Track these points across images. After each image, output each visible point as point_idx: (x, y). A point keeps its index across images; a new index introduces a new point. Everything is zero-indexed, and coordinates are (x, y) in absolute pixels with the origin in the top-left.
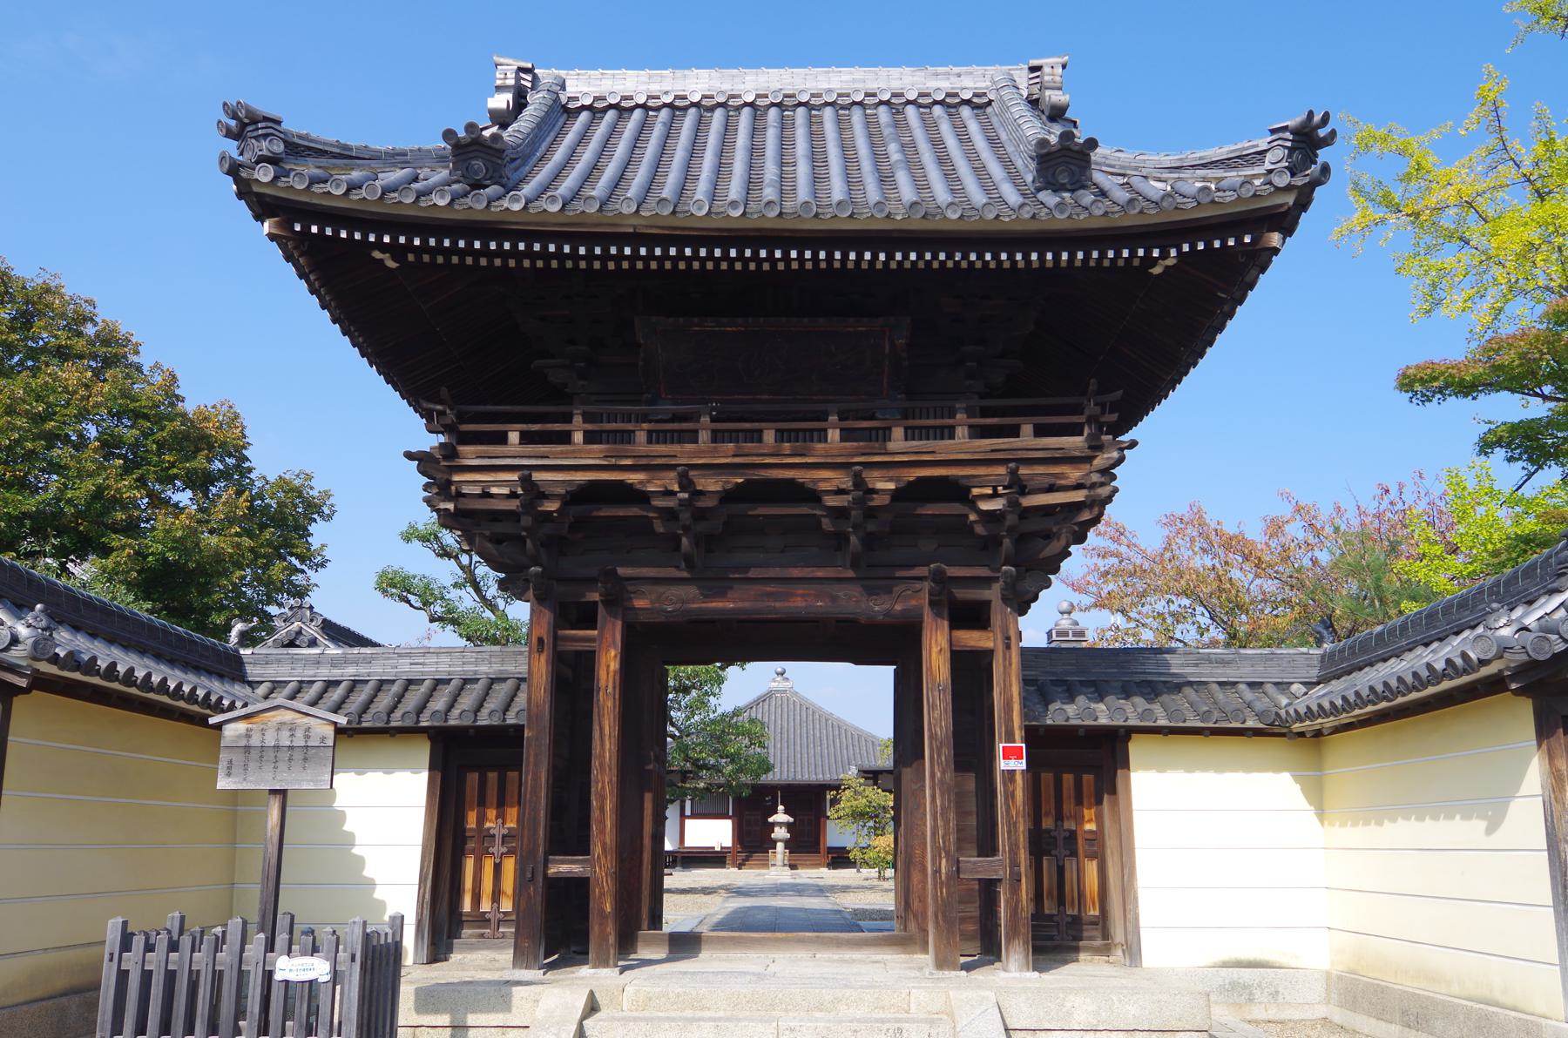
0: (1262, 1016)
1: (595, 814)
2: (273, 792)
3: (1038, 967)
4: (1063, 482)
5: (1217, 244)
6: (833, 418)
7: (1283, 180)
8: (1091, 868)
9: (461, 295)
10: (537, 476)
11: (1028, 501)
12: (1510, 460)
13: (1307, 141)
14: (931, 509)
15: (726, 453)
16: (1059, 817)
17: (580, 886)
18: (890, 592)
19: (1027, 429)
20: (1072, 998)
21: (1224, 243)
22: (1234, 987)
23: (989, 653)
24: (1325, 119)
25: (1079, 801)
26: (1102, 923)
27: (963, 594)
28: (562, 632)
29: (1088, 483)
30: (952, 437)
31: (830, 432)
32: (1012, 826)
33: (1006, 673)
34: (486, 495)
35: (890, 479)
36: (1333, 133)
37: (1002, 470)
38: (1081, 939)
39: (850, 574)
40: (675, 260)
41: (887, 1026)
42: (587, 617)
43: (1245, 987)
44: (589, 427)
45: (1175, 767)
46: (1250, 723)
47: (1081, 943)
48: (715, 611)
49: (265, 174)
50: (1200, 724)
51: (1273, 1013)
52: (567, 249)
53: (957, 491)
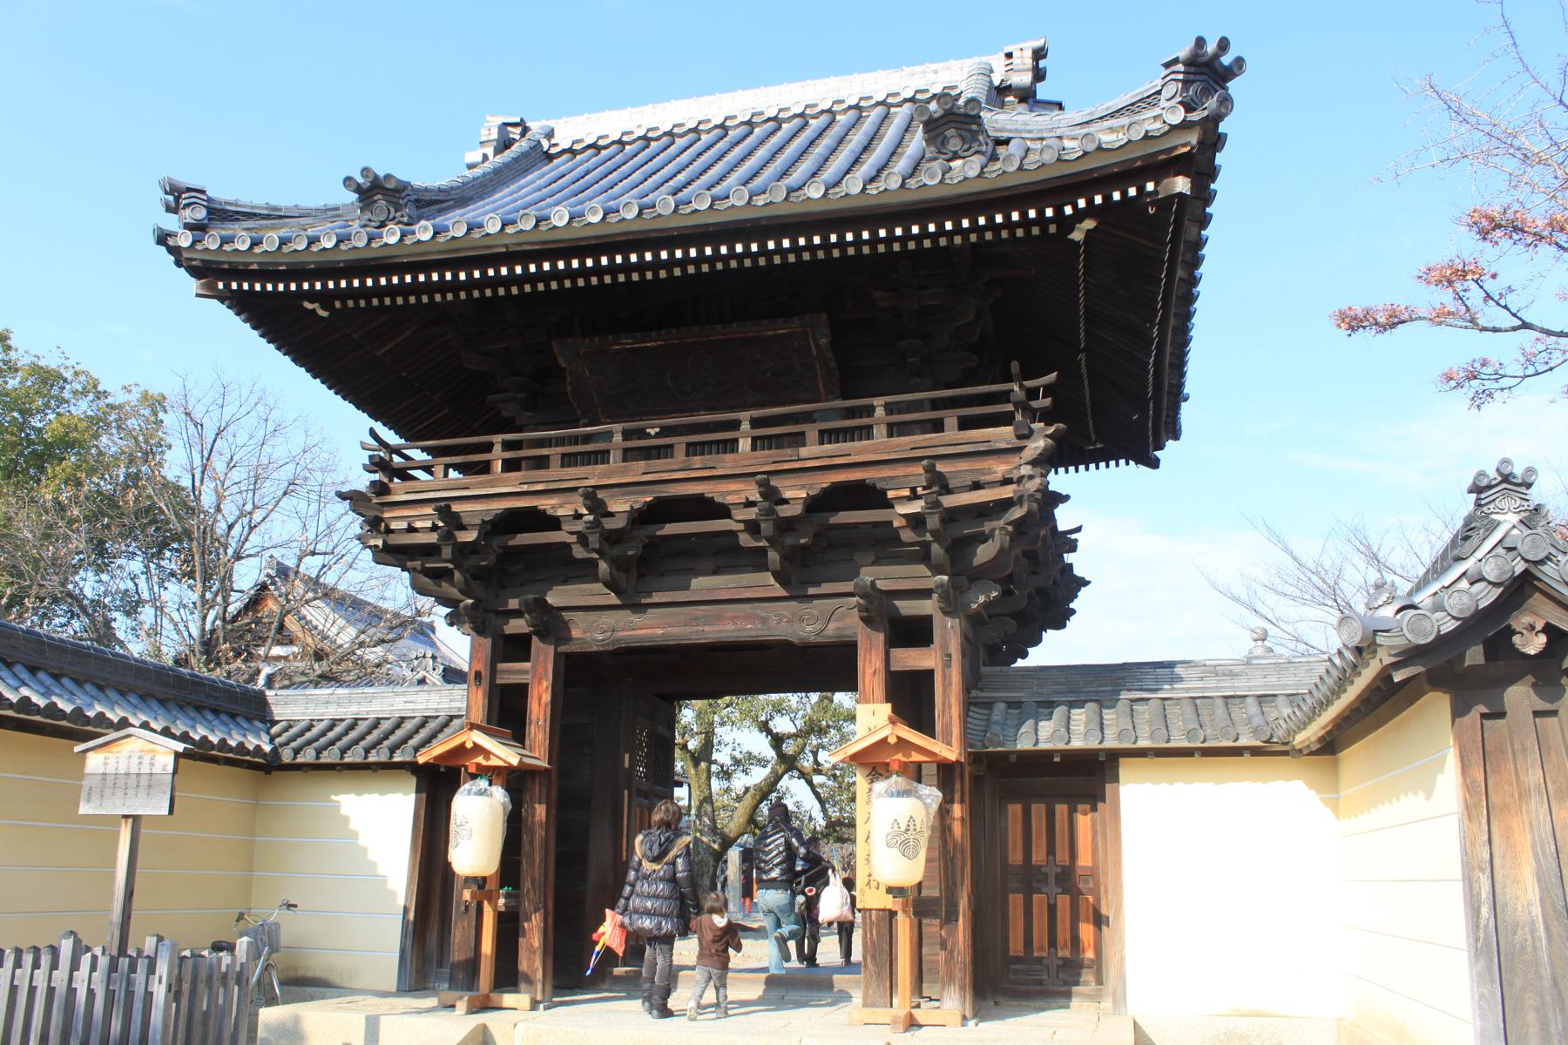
5: (1117, 196)
6: (745, 426)
7: (1178, 116)
9: (430, 331)
10: (456, 508)
14: (671, 529)
15: (638, 471)
19: (951, 421)
21: (1124, 194)
23: (929, 674)
24: (1224, 45)
26: (1098, 966)
27: (907, 607)
28: (501, 666)
29: (1015, 476)
31: (741, 441)
33: (945, 694)
34: (411, 529)
35: (803, 487)
36: (1239, 62)
37: (918, 469)
38: (1077, 984)
40: (918, 239)
42: (516, 648)
44: (508, 455)
47: (1075, 989)
49: (185, 240)
50: (1185, 744)
52: (1032, 214)
53: (871, 496)
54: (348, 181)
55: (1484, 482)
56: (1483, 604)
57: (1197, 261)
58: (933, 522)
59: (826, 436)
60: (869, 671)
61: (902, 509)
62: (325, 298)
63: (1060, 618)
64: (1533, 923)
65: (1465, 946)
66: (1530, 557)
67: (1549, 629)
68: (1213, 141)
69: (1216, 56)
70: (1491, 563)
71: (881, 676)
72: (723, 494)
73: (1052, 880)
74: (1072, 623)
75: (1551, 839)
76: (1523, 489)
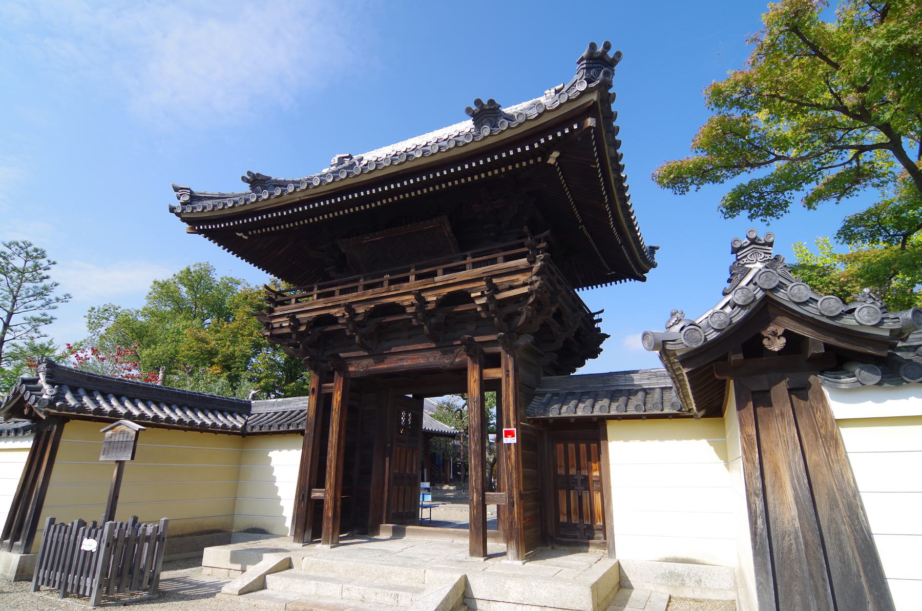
0: (690, 595)
1: (328, 469)
2: (117, 462)
3: (530, 558)
4: (516, 283)
5: (559, 134)
7: (583, 87)
8: (597, 497)
10: (298, 316)
11: (500, 296)
12: (751, 217)
13: (600, 63)
16: (579, 468)
17: (320, 502)
18: (453, 352)
19: (500, 259)
20: (509, 582)
22: (672, 575)
23: (499, 380)
24: (607, 46)
25: (589, 459)
26: (603, 529)
27: (488, 350)
30: (465, 269)
32: (510, 475)
33: (507, 390)
34: (281, 327)
36: (618, 54)
39: (434, 345)
41: (392, 592)
43: (679, 575)
45: (670, 438)
46: (666, 411)
48: (379, 369)
51: (697, 595)
53: (464, 297)
54: (243, 178)
55: (738, 245)
56: (735, 320)
57: (621, 168)
58: (491, 307)
59: (445, 272)
60: (472, 380)
61: (478, 302)
62: (244, 229)
63: (594, 353)
64: (796, 532)
65: (861, 494)
66: (766, 287)
67: (786, 334)
68: (607, 99)
69: (604, 53)
70: (746, 291)
71: (478, 382)
72: (403, 301)
73: (579, 482)
74: (601, 356)
75: (804, 474)
76: (767, 247)
